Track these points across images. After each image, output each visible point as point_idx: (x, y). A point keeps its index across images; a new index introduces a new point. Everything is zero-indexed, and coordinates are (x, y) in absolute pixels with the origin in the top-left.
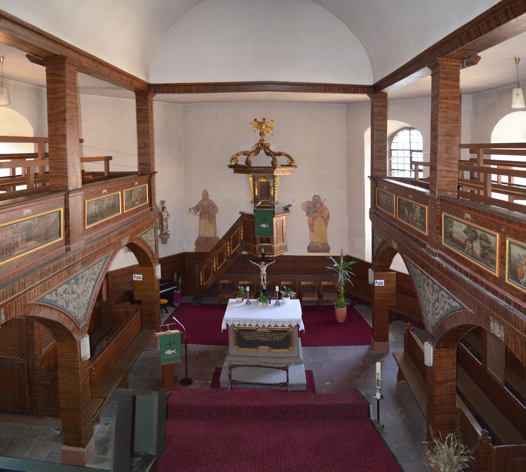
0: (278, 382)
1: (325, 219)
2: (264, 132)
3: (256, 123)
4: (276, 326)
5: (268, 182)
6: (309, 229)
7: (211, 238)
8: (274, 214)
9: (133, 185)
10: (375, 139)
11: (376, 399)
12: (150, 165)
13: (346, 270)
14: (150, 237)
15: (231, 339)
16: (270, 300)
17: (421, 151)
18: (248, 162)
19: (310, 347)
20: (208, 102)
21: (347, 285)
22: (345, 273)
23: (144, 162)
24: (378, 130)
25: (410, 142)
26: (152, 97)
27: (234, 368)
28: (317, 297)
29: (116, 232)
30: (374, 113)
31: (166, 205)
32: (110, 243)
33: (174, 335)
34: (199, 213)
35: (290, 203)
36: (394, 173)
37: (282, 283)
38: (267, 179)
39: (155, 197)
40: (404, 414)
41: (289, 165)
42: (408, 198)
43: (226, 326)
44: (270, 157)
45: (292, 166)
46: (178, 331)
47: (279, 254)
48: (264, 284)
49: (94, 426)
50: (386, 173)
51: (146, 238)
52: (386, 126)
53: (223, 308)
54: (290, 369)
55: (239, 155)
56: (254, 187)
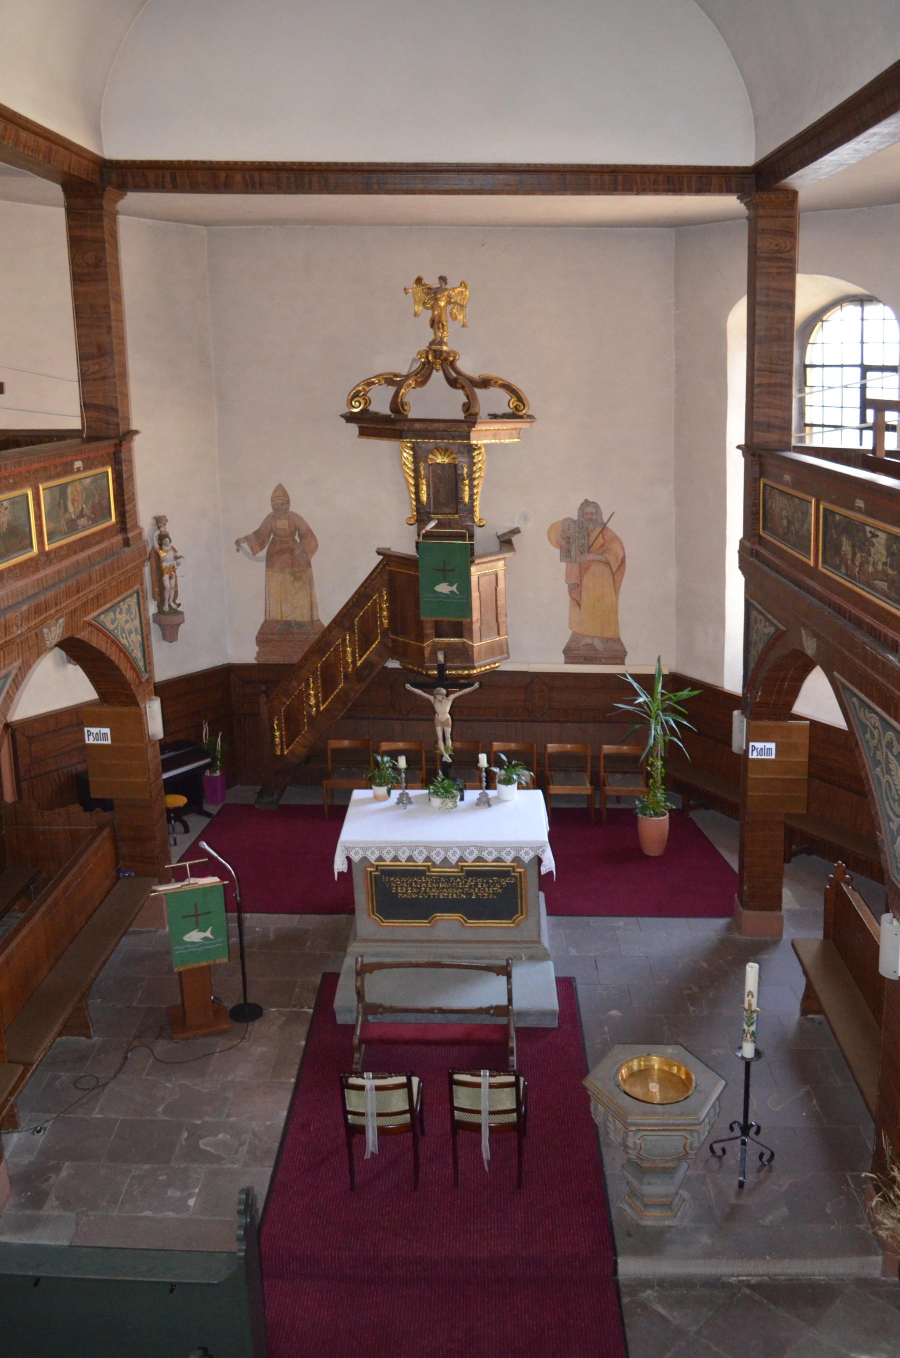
0: (485, 1004)
1: (614, 570)
2: (443, 316)
3: (420, 289)
4: (479, 859)
5: (456, 466)
6: (568, 598)
7: (300, 625)
8: (472, 554)
9: (67, 469)
10: (760, 333)
11: (743, 1058)
12: (115, 410)
13: (673, 715)
14: (127, 621)
15: (362, 897)
16: (461, 791)
17: (893, 369)
18: (397, 406)
19: (569, 918)
20: (281, 222)
21: (672, 752)
22: (667, 722)
23: (96, 402)
24: (767, 304)
25: (862, 342)
26: (116, 201)
27: (371, 972)
28: (588, 785)
29: (25, 608)
30: (758, 255)
31: (169, 528)
32: (8, 638)
33: (206, 889)
34: (263, 553)
35: (515, 525)
36: (811, 434)
37: (497, 746)
38: (452, 456)
39: (135, 506)
40: (814, 1101)
41: (513, 416)
42: (852, 508)
43: (346, 862)
44: (460, 393)
45: (521, 417)
46: (216, 879)
47: (488, 667)
48: (446, 749)
49: (4, 1137)
50: (791, 436)
51: (113, 622)
52: (792, 293)
53: (338, 814)
54: (516, 972)
55: (373, 383)
56: (417, 478)
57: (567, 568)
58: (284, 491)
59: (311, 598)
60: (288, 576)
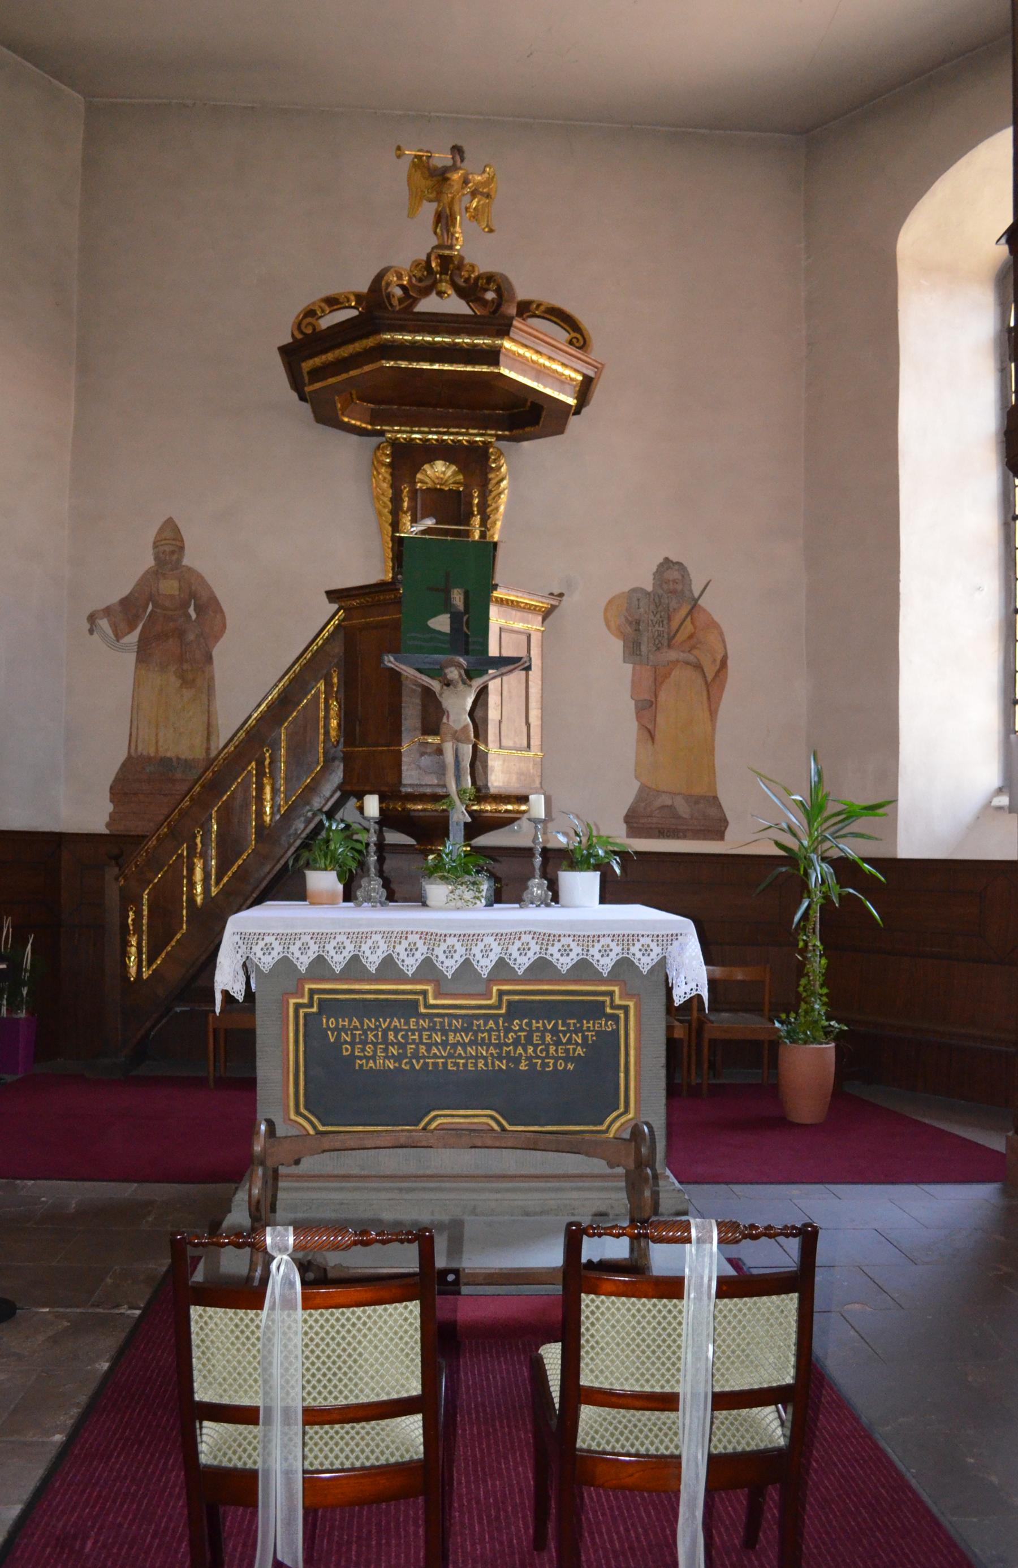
1: (709, 679)
6: (635, 725)
34: (134, 637)
57: (634, 675)
58: (176, 530)
59: (209, 717)
60: (173, 679)
